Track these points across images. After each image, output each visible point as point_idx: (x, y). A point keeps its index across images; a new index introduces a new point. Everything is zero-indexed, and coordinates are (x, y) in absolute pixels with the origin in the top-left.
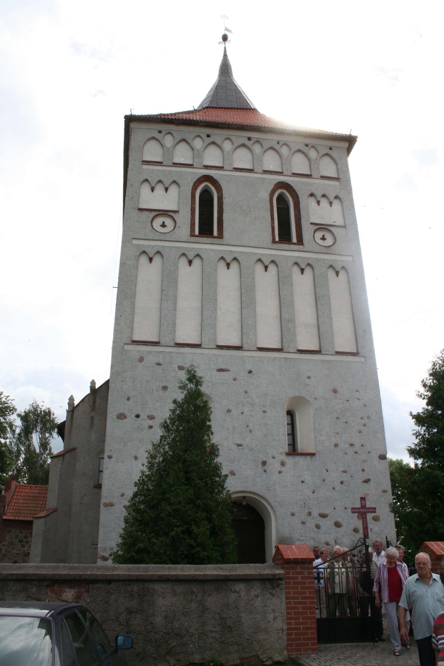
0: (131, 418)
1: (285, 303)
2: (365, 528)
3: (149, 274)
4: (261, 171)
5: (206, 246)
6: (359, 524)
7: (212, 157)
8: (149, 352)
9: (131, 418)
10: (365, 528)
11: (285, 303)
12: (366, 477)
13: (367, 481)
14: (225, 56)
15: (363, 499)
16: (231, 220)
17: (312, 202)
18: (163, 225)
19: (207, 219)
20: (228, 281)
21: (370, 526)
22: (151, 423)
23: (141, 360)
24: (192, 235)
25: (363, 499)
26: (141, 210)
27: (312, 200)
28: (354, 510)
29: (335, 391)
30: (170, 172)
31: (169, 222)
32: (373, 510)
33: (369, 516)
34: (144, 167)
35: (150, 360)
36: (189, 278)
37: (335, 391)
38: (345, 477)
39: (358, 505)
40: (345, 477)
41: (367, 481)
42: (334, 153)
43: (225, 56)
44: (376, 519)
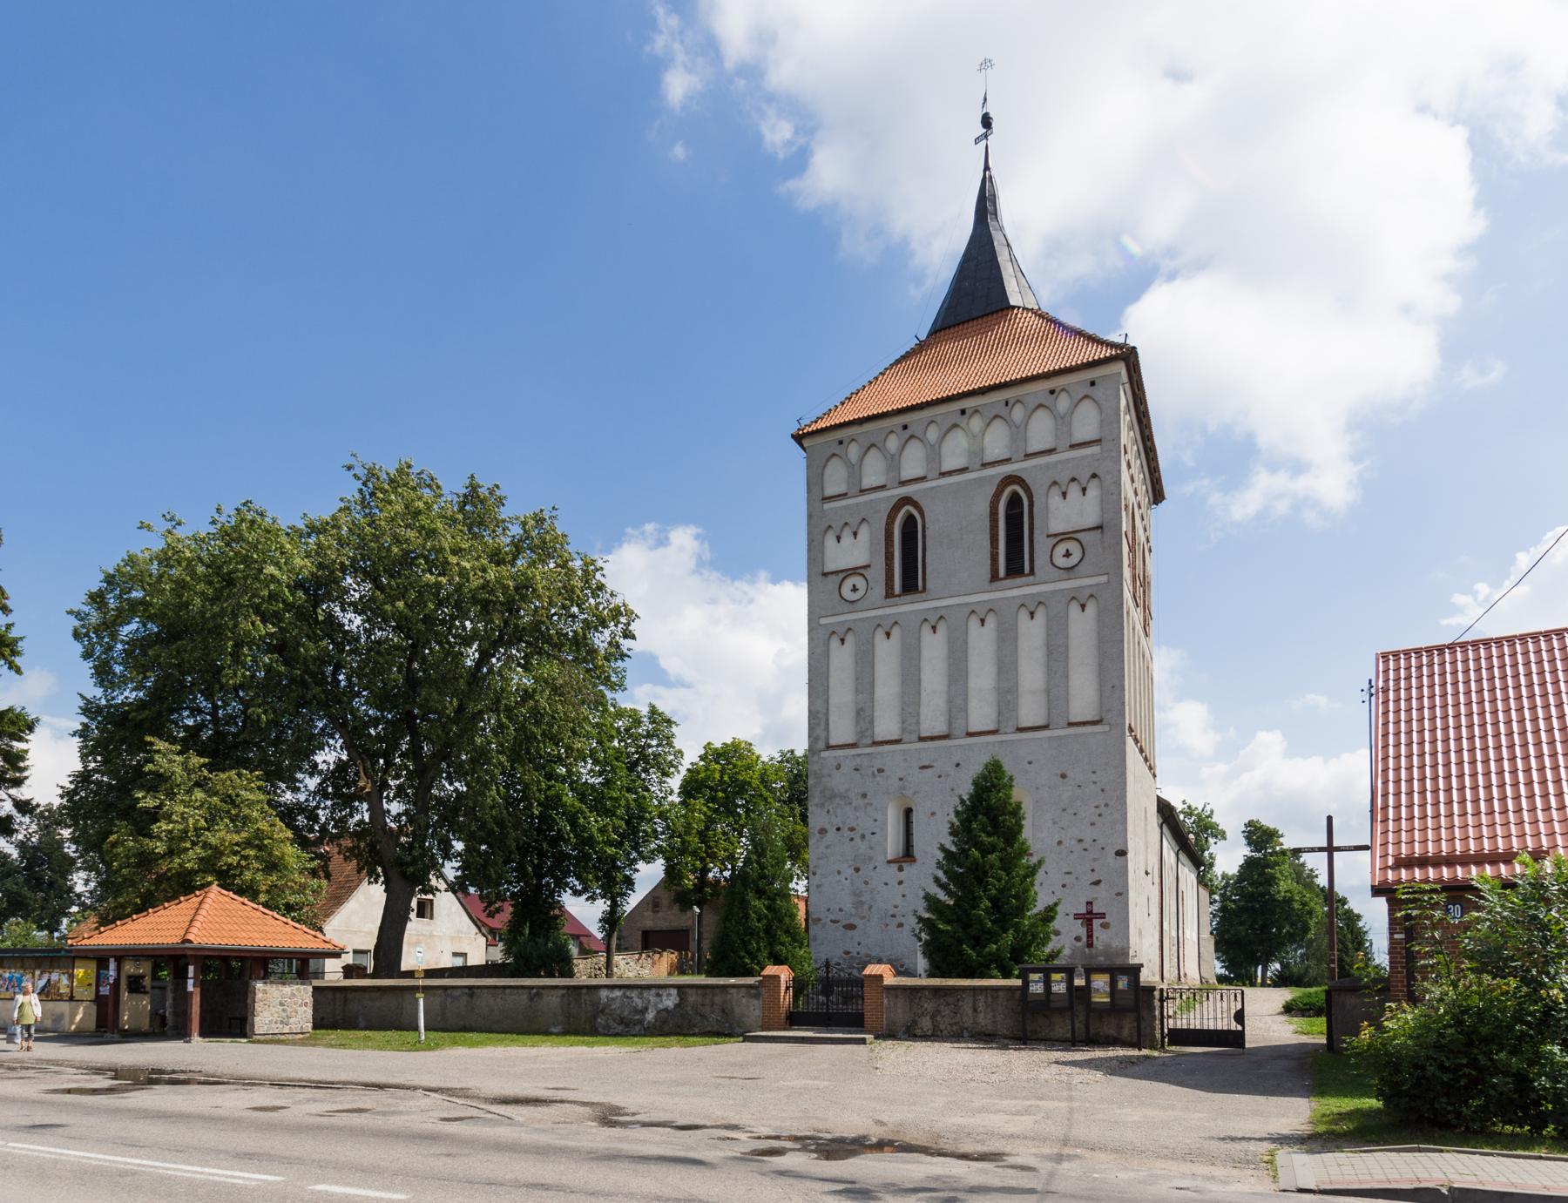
0: (832, 833)
1: (1007, 667)
2: (1090, 936)
3: (842, 658)
4: (978, 466)
5: (908, 607)
6: (1083, 932)
7: (996, 442)
8: (846, 757)
9: (832, 833)
10: (1090, 936)
11: (1007, 667)
12: (1095, 877)
13: (1097, 883)
14: (986, 206)
15: (1089, 903)
16: (937, 560)
17: (1055, 499)
18: (855, 589)
19: (908, 568)
20: (934, 647)
21: (1095, 934)
22: (852, 834)
23: (838, 767)
24: (889, 594)
25: (1089, 903)
26: (825, 575)
27: (1055, 492)
28: (1077, 917)
29: (1063, 776)
30: (857, 505)
31: (858, 581)
32: (1103, 916)
33: (1096, 923)
34: (827, 506)
35: (847, 766)
36: (887, 653)
37: (1063, 776)
38: (1068, 879)
39: (1083, 910)
40: (1068, 879)
41: (1097, 883)
42: (1098, 392)
43: (986, 206)
44: (1105, 926)
